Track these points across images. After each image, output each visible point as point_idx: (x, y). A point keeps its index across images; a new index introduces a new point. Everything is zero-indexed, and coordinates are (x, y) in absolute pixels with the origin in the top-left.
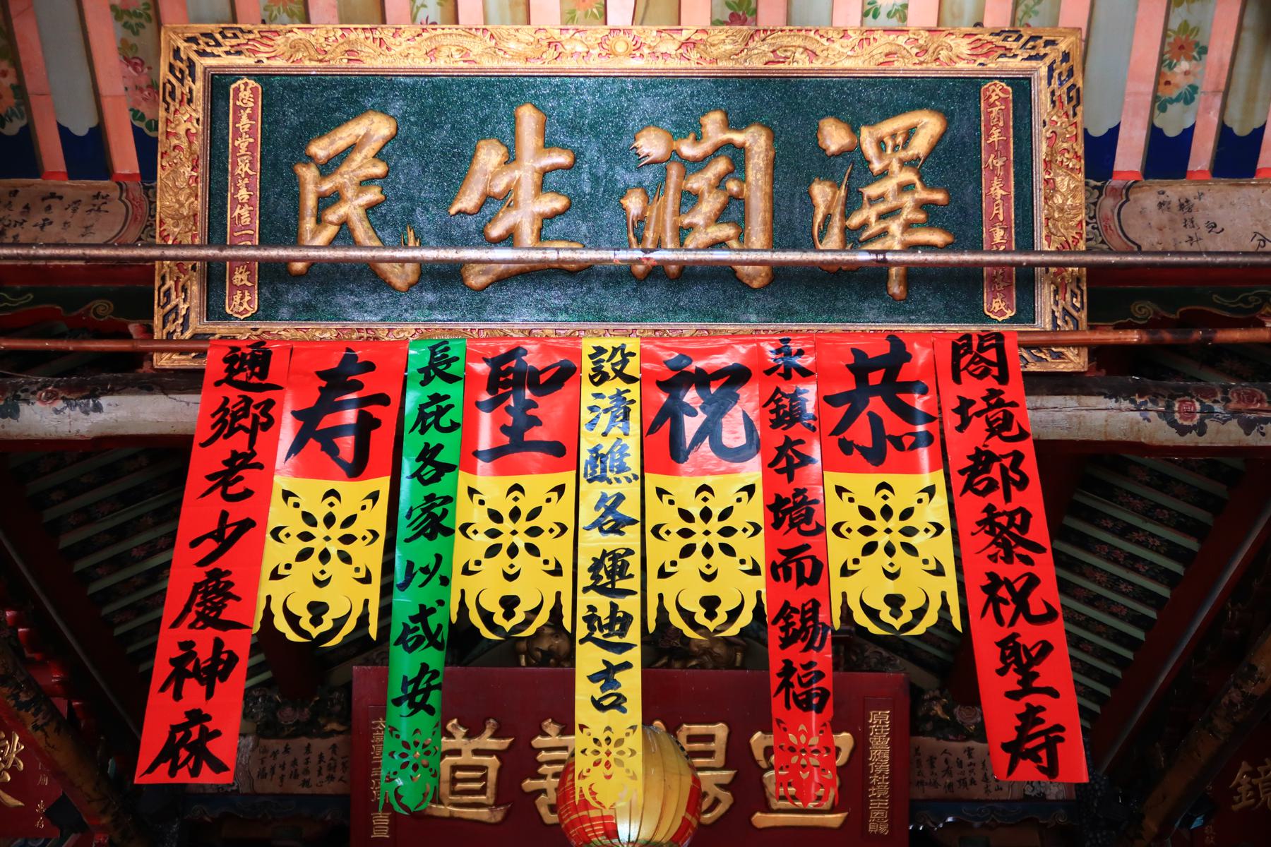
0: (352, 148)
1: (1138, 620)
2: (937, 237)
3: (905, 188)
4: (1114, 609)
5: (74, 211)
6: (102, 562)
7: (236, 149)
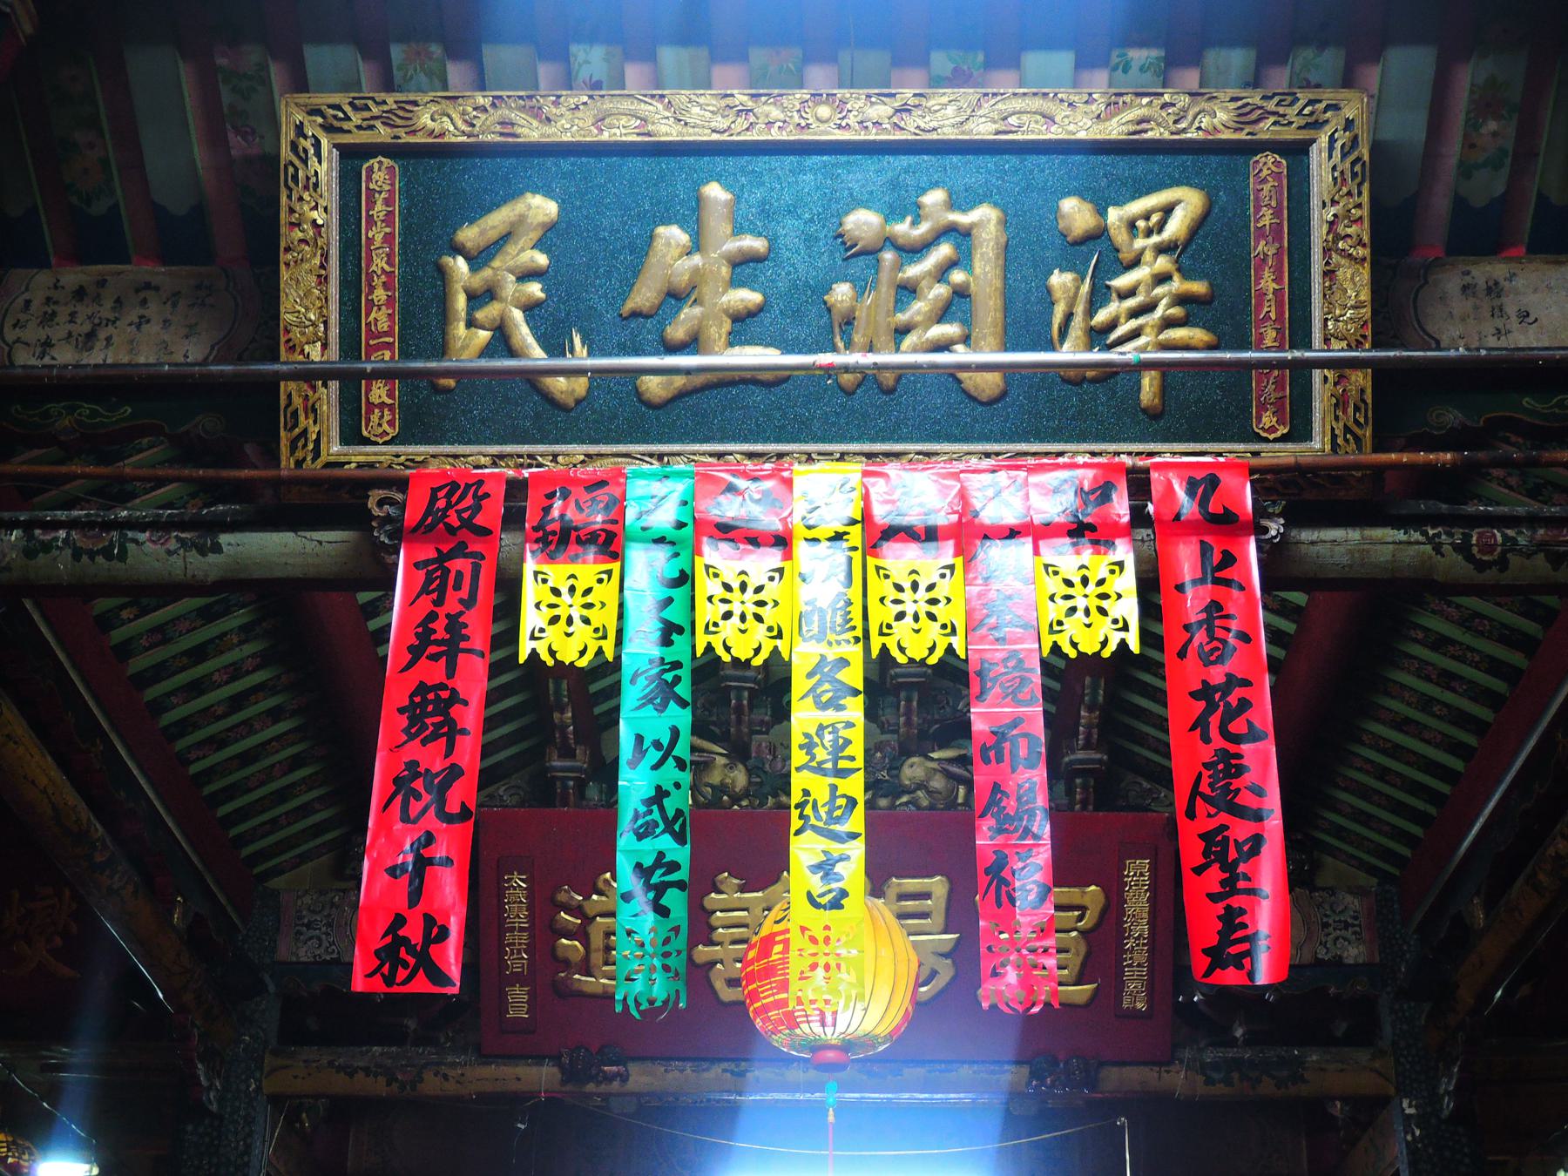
0: (506, 238)
1: (1456, 748)
2: (1196, 334)
3: (1162, 279)
4: (1427, 735)
5: (174, 305)
6: (177, 689)
7: (370, 241)
